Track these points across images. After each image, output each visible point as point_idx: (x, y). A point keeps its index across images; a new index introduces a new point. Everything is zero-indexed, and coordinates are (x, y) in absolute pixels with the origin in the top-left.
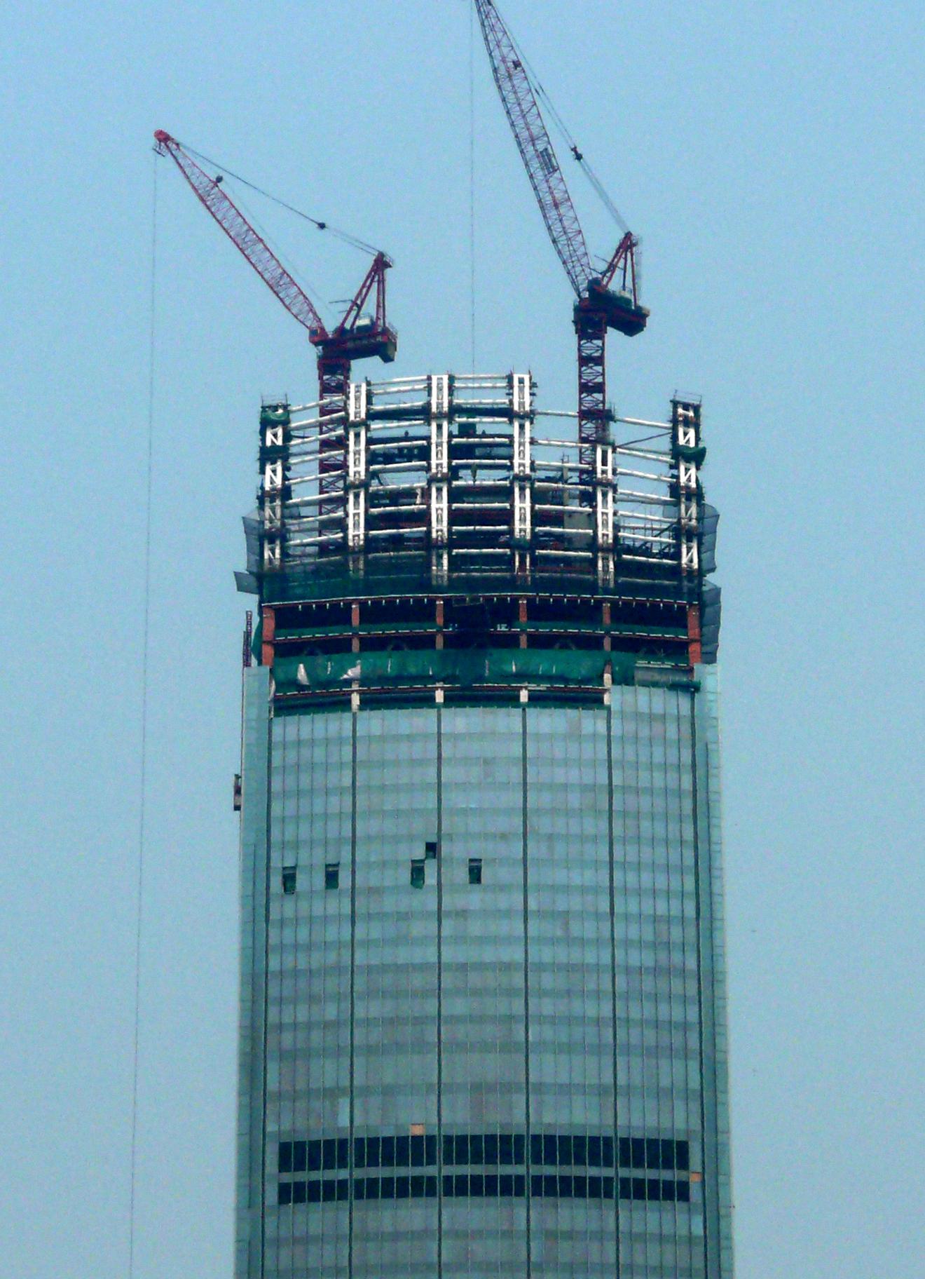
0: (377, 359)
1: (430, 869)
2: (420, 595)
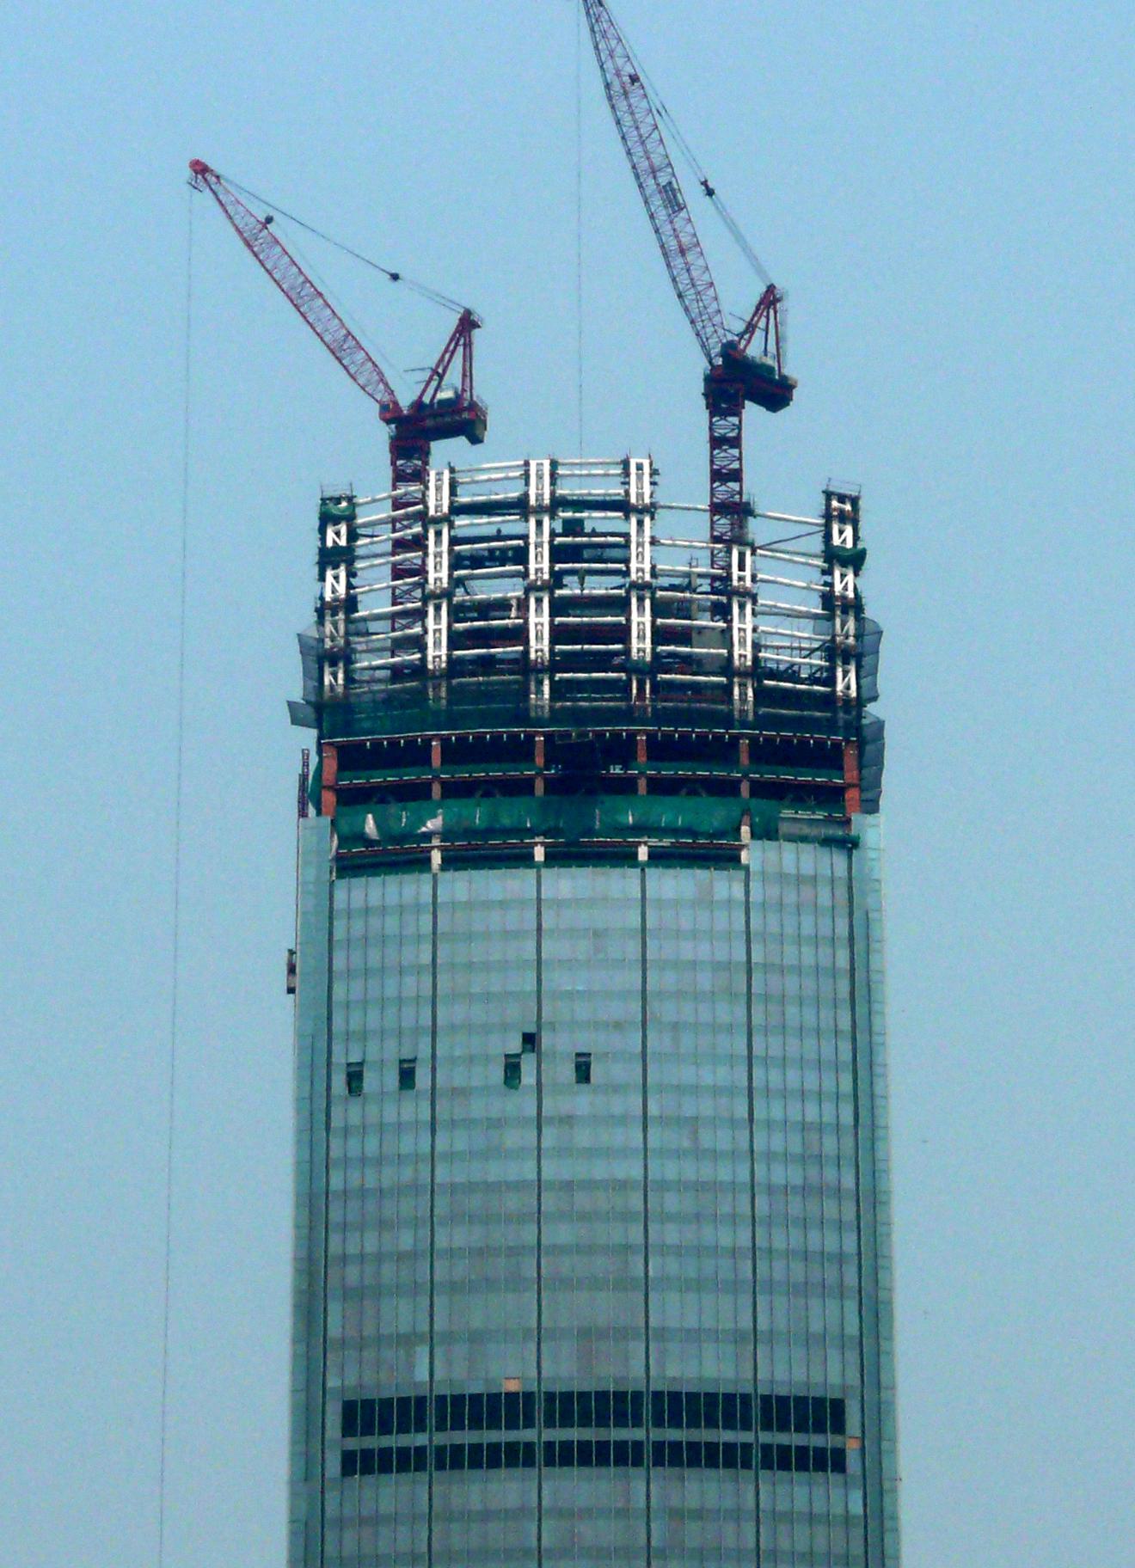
0: (462, 441)
1: (528, 1065)
2: (516, 730)
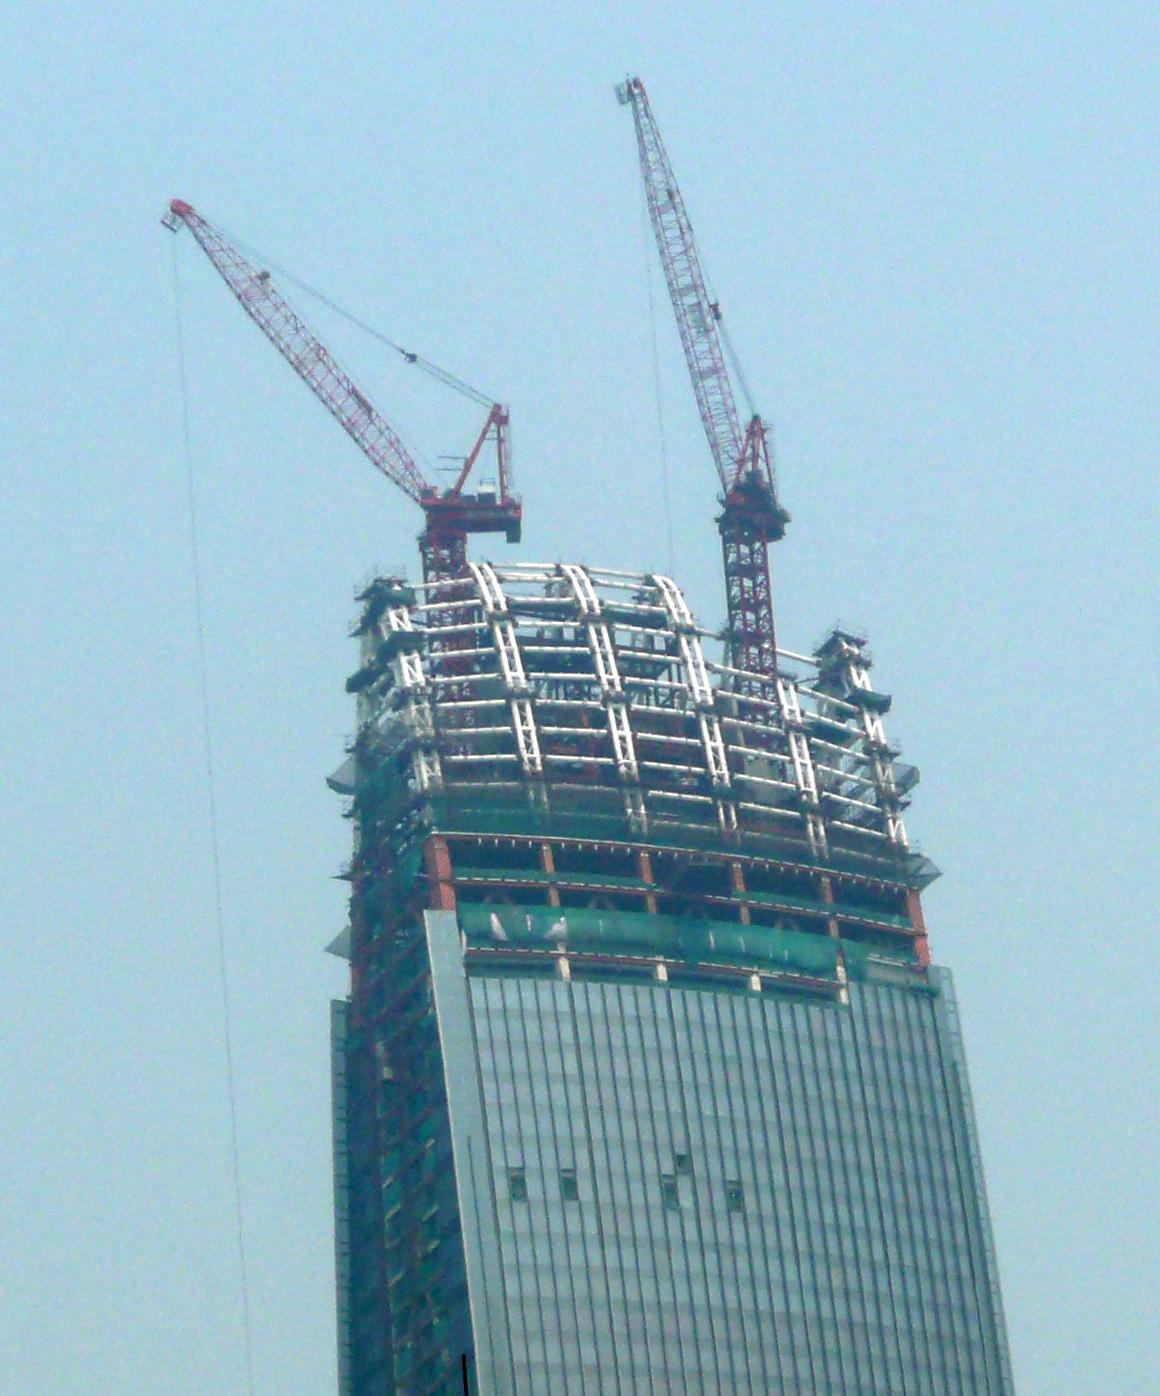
0: (500, 537)
1: (684, 1185)
2: (507, 835)
